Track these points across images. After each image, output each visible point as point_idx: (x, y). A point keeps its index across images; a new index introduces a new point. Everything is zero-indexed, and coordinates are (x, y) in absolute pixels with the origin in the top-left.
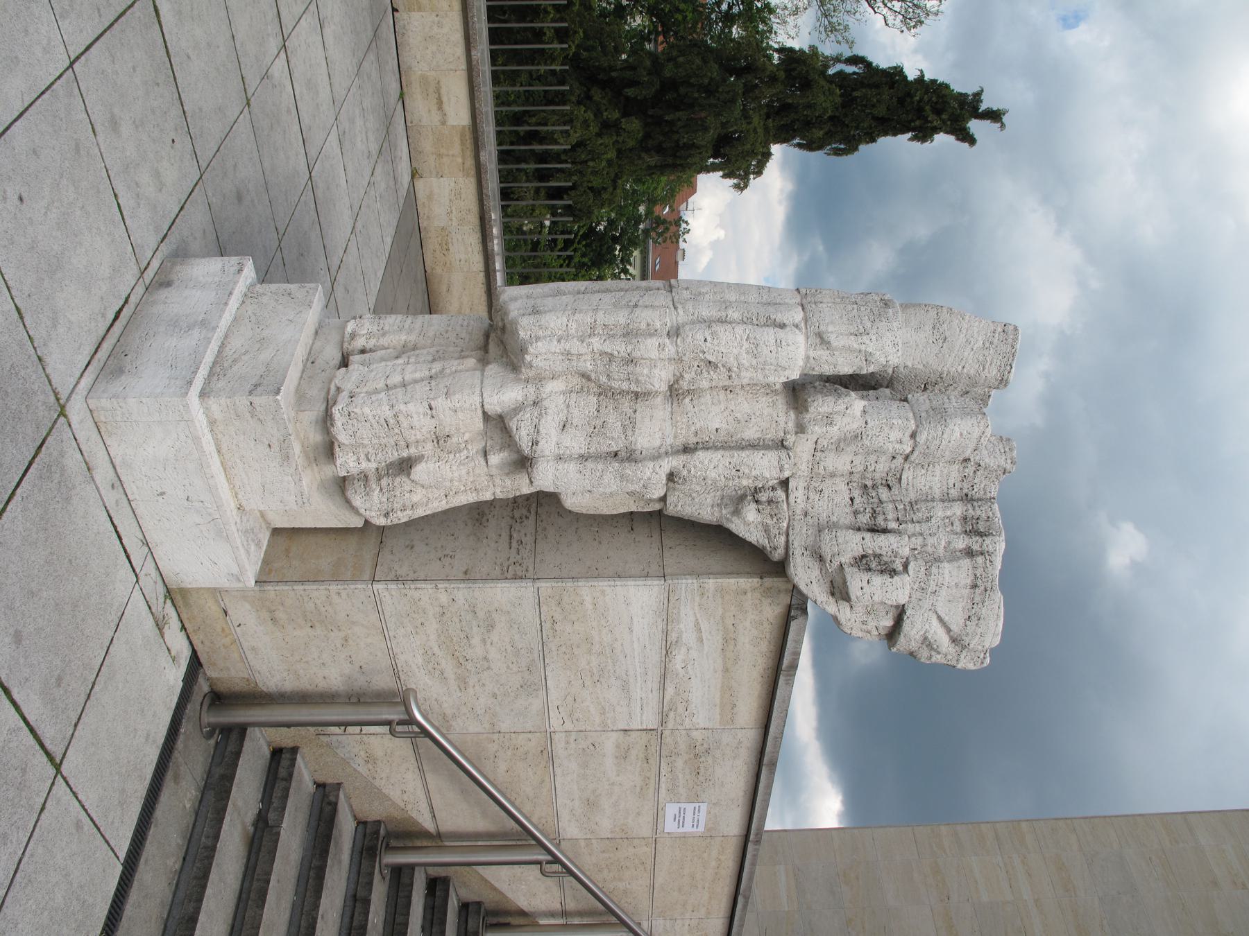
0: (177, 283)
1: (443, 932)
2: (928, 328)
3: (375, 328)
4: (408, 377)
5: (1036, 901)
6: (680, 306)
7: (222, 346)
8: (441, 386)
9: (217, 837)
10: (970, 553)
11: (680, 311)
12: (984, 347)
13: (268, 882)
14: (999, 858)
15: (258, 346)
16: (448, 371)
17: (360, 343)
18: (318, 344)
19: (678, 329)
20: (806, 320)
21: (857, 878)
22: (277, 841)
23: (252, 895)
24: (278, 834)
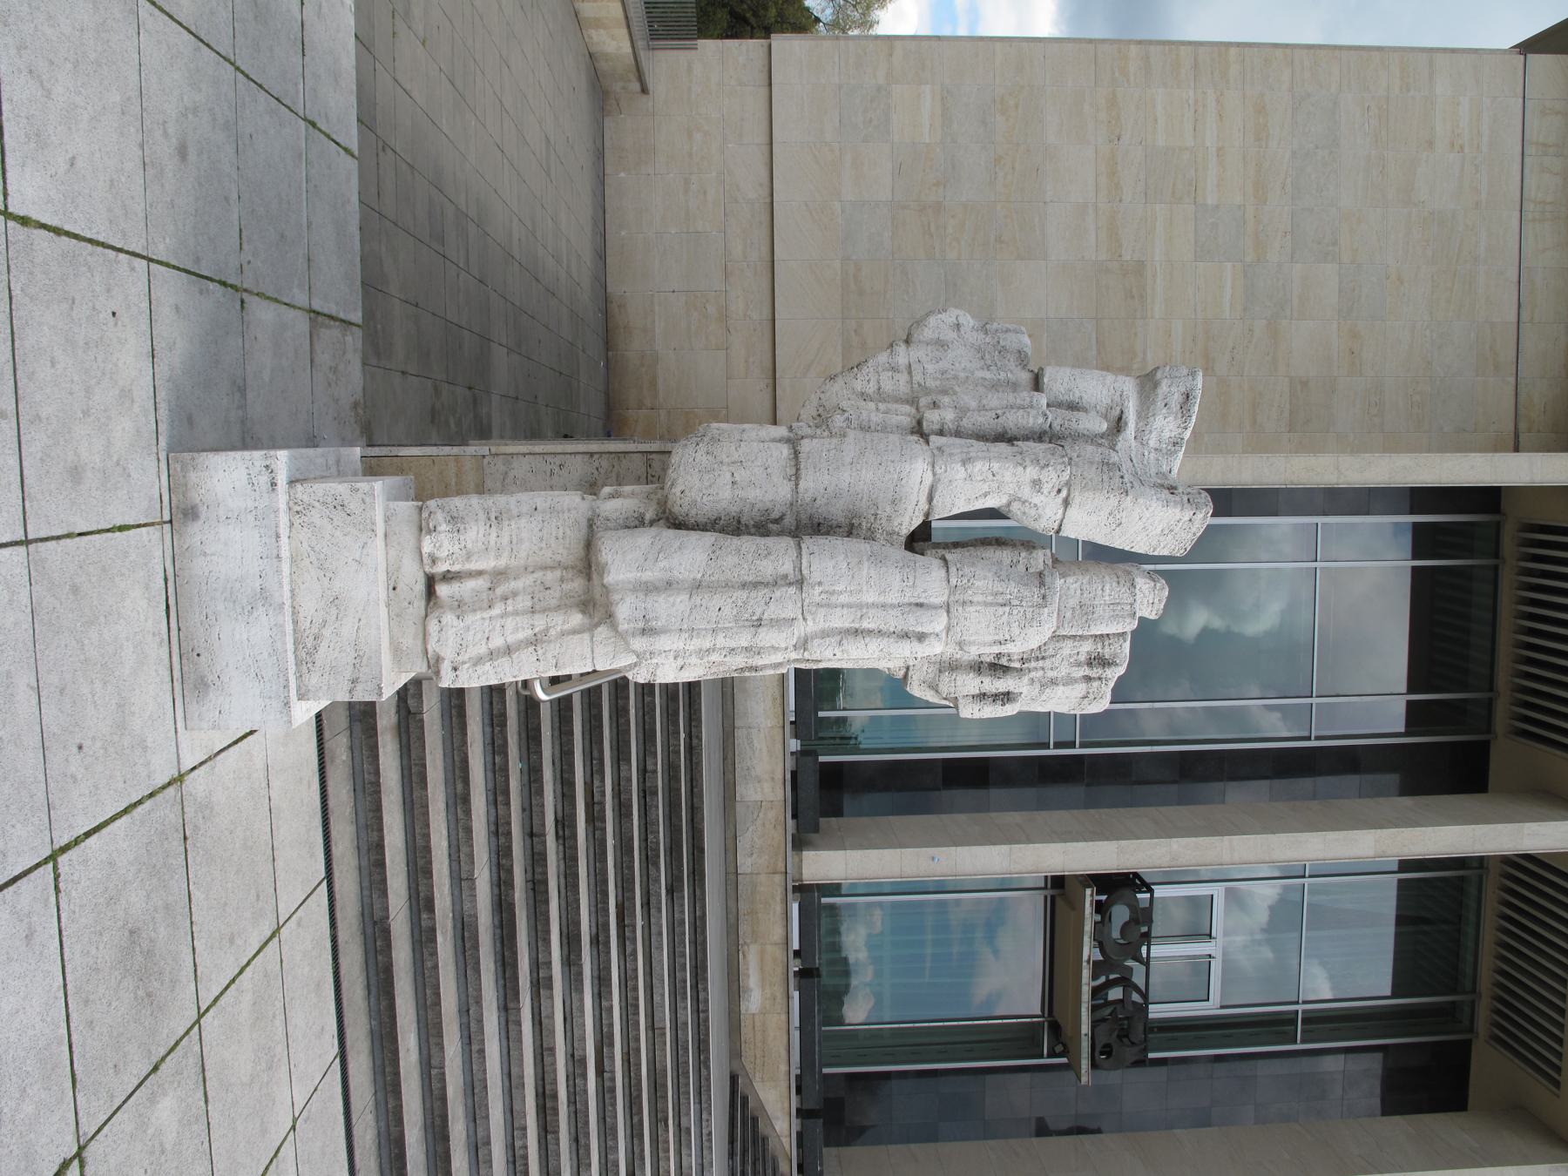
0: (203, 510)
1: (617, 1173)
2: (1104, 513)
3: (457, 547)
4: (511, 639)
5: (1219, 149)
6: (809, 618)
7: (295, 622)
8: (549, 656)
9: (377, 773)
10: (1088, 679)
11: (810, 623)
12: (1162, 533)
13: (424, 766)
14: (1191, 93)
15: (334, 611)
16: (552, 632)
17: (441, 568)
18: (392, 552)
19: (806, 641)
20: (948, 629)
21: (1017, 106)
22: (422, 728)
23: (414, 778)
24: (422, 721)
